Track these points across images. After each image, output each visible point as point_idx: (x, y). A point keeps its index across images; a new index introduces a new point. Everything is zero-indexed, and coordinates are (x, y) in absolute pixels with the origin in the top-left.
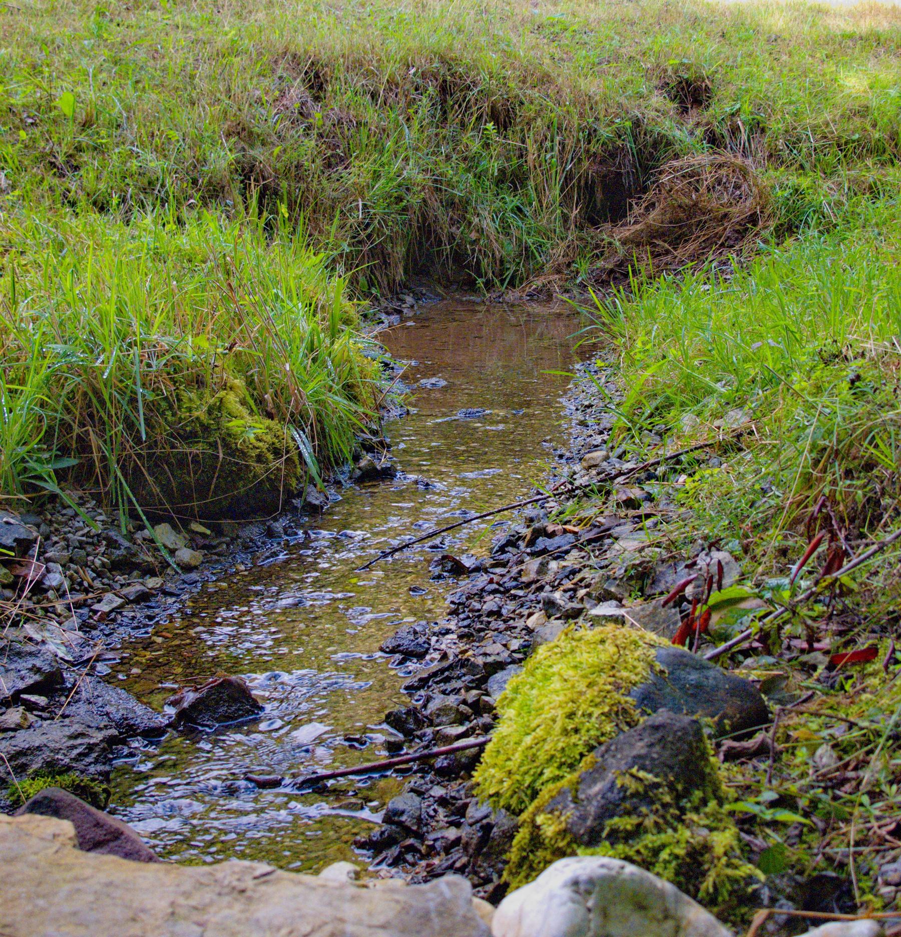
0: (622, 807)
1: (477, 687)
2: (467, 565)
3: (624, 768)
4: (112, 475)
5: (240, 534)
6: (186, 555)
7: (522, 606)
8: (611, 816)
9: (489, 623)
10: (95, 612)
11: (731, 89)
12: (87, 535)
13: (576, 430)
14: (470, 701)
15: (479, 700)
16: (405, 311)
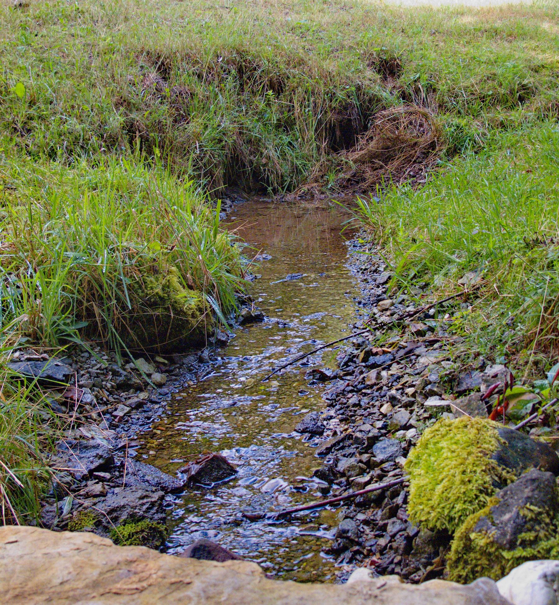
0: (526, 527)
1: (366, 452)
2: (329, 375)
3: (522, 505)
4: (110, 332)
5: (185, 361)
6: (158, 377)
7: (372, 399)
8: (520, 532)
9: (355, 411)
10: (116, 417)
11: (413, 65)
12: (100, 369)
13: (362, 285)
14: (364, 461)
15: (369, 460)
16: (227, 209)
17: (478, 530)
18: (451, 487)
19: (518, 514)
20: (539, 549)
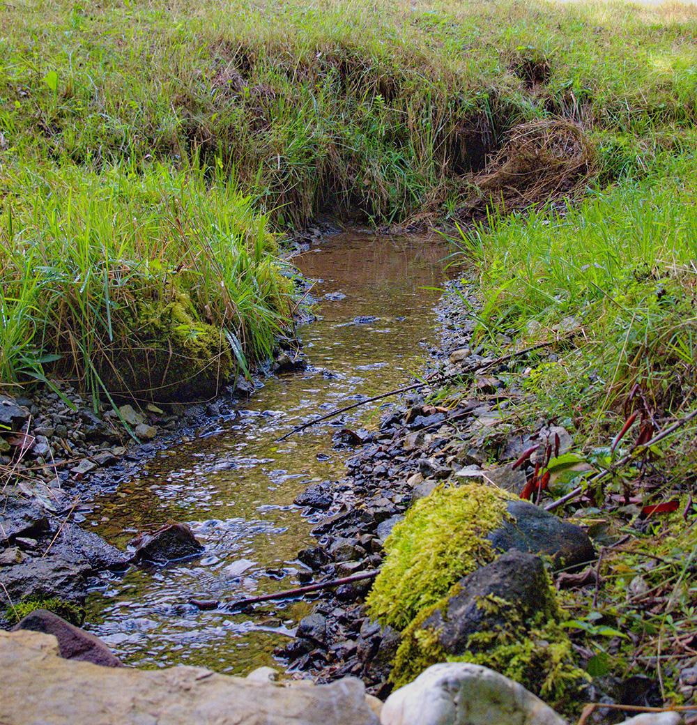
4: (87, 367)
6: (144, 429)
7: (404, 469)
8: (473, 632)
10: (74, 474)
13: (446, 333)
14: (363, 543)
16: (313, 240)
17: (425, 626)
18: (421, 573)
19: (474, 606)
20: (494, 655)
